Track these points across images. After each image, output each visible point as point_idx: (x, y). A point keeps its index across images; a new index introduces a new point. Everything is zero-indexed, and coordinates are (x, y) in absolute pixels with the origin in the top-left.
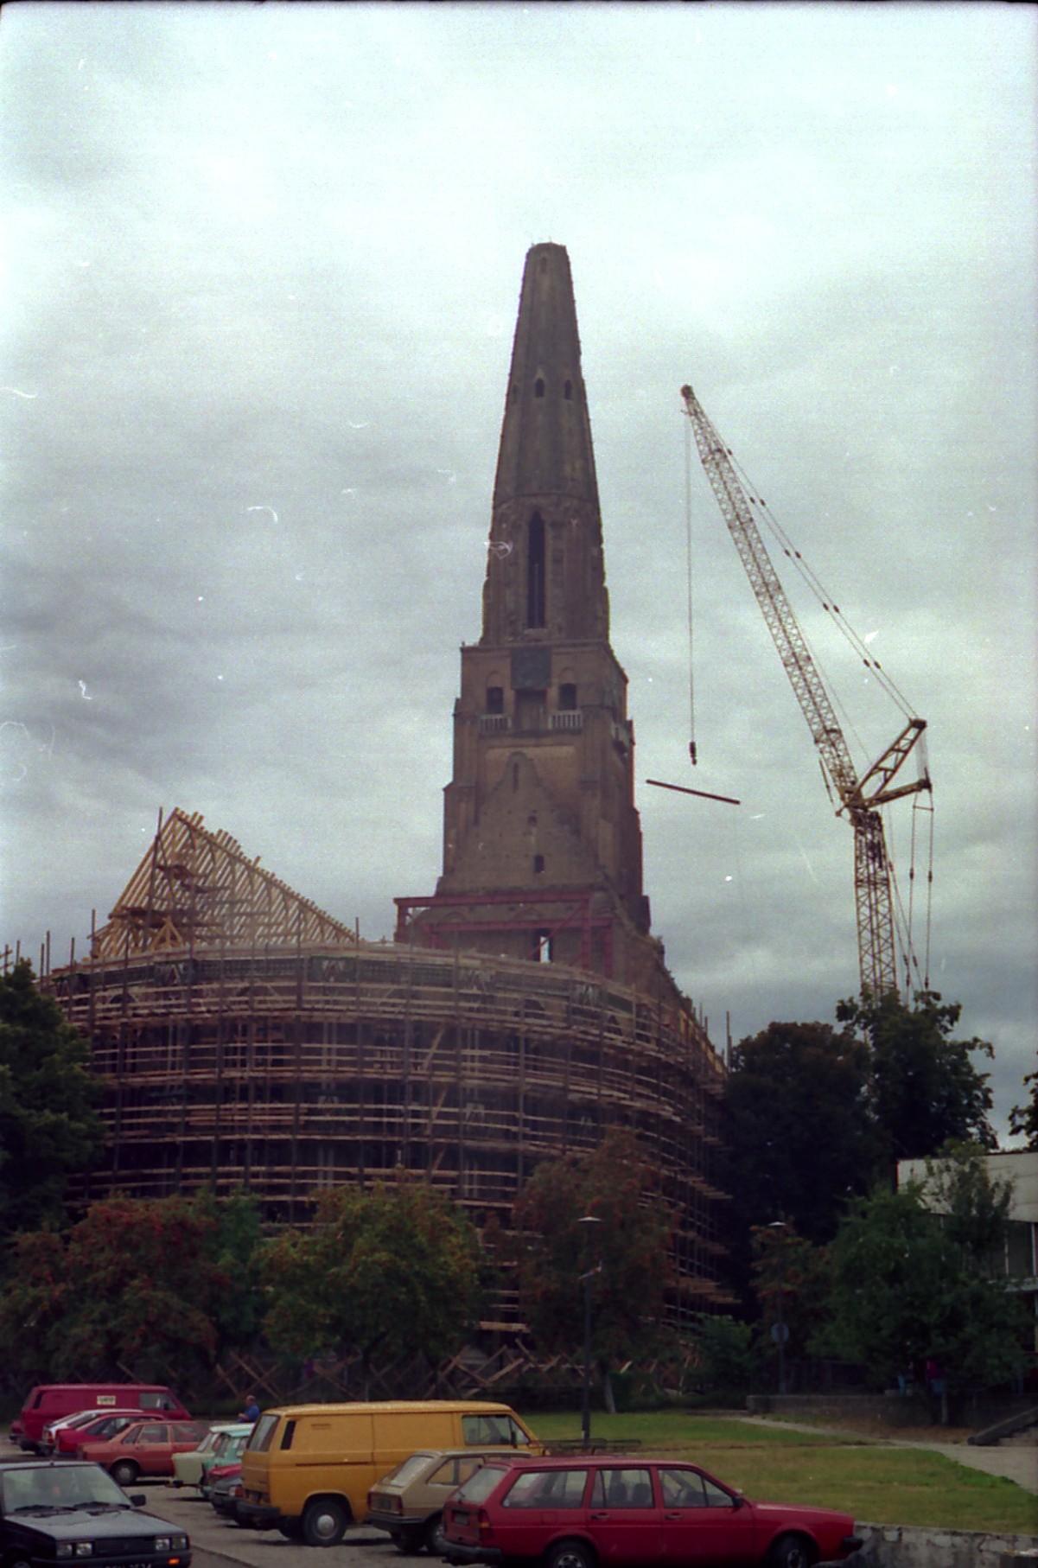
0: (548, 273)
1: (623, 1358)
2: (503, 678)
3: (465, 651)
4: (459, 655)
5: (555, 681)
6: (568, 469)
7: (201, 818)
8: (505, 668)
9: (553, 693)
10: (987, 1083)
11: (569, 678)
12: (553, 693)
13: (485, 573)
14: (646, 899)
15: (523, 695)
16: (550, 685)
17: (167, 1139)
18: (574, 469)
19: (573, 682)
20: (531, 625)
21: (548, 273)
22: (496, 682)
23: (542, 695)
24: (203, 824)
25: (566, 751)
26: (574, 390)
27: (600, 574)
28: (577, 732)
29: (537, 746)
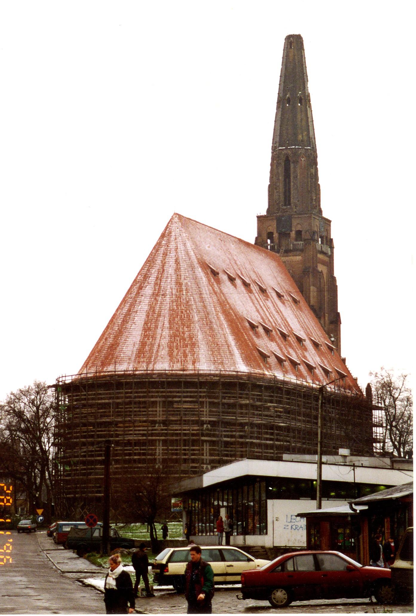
0: (294, 45)
1: (284, 491)
2: (272, 227)
3: (258, 217)
4: (256, 219)
5: (293, 229)
6: (300, 137)
7: (12, 394)
8: (274, 224)
9: (293, 234)
10: (15, 392)
11: (299, 228)
12: (293, 234)
13: (268, 180)
14: (339, 313)
15: (281, 234)
16: (291, 231)
17: (381, 557)
18: (303, 136)
19: (301, 229)
20: (285, 205)
21: (294, 45)
22: (271, 229)
23: (288, 235)
24: (264, 213)
25: (299, 258)
26: (305, 100)
27: (317, 179)
28: (302, 250)
29: (287, 256)
